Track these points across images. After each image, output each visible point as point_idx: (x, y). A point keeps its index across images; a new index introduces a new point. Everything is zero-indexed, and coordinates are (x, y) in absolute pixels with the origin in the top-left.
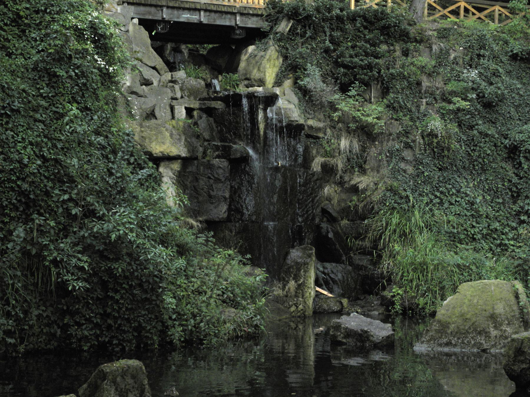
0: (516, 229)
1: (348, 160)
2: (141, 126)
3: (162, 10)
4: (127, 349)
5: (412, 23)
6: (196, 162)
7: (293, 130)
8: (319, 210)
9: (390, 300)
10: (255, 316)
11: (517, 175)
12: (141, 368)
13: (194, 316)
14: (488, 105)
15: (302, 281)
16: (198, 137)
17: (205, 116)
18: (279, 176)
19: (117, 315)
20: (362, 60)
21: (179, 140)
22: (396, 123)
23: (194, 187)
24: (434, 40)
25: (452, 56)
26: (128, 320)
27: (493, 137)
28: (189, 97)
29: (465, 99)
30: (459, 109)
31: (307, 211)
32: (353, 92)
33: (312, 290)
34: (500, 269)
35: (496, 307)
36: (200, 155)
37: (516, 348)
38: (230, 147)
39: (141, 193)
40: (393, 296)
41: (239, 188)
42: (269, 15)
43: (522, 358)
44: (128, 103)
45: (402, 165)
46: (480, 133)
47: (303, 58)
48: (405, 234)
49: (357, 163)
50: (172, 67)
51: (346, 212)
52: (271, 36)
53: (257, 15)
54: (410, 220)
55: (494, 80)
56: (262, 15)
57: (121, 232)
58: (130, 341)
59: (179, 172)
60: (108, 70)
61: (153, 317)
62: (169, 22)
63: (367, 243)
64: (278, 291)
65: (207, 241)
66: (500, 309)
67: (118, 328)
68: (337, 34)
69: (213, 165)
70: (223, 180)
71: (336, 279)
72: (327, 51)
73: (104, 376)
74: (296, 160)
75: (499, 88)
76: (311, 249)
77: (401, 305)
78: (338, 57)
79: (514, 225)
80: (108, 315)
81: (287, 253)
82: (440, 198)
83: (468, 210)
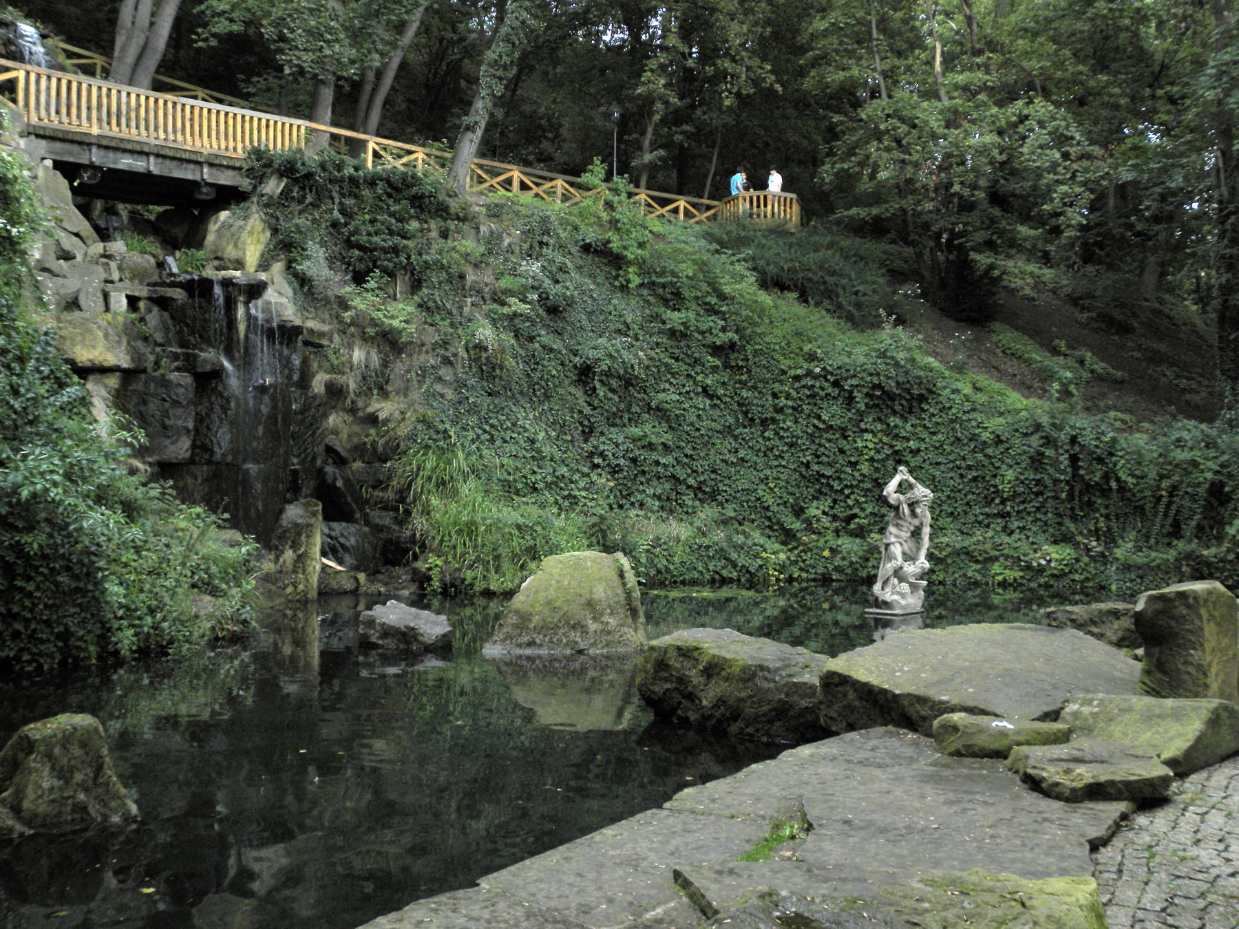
0: (588, 475)
1: (364, 378)
2: (59, 320)
3: (90, 150)
4: (46, 667)
5: (452, 195)
6: (143, 376)
7: (287, 334)
8: (321, 448)
9: (424, 575)
10: (243, 607)
11: (589, 404)
12: (96, 729)
13: (152, 611)
14: (553, 310)
15: (302, 550)
16: (146, 339)
17: (156, 309)
18: (266, 399)
19: (29, 615)
20: (384, 240)
21: (119, 342)
22: (431, 329)
23: (141, 413)
24: (482, 219)
25: (506, 243)
26: (48, 623)
27: (560, 352)
28: (131, 279)
29: (523, 301)
30: (515, 315)
31: (306, 449)
32: (372, 284)
33: (318, 562)
34: (570, 529)
35: (594, 590)
36: (150, 366)
37: (657, 660)
38: (195, 356)
39: (64, 422)
40: (430, 569)
41: (208, 415)
42: (251, 169)
43: (666, 675)
44: (37, 286)
45: (438, 387)
46: (543, 347)
47: (301, 232)
48: (444, 483)
49: (378, 384)
50: (104, 235)
51: (359, 450)
52: (255, 199)
53: (234, 168)
54: (450, 463)
55: (560, 277)
56: (240, 169)
57: (39, 487)
58: (50, 655)
59: (117, 390)
60: (9, 232)
61: (89, 616)
62: (99, 168)
63: (390, 495)
64: (268, 566)
65: (163, 494)
66: (600, 592)
67: (30, 637)
68: (349, 202)
69: (169, 381)
70: (185, 403)
71: (348, 544)
72: (335, 225)
73: (29, 746)
74: (289, 377)
75: (568, 289)
76: (316, 505)
77: (441, 580)
78: (352, 234)
79: (586, 470)
80: (15, 616)
81: (281, 511)
82: (490, 433)
83: (527, 450)
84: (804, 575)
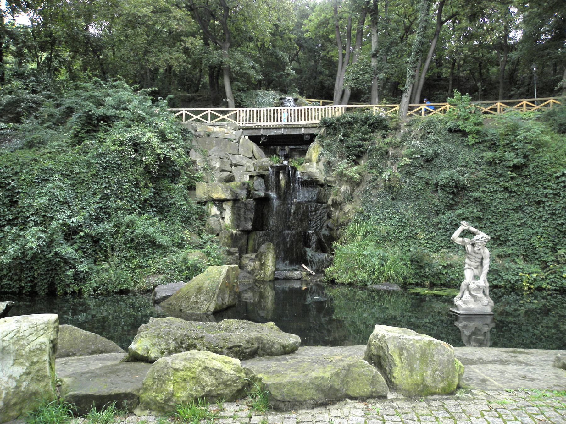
59: (232, 207)
62: (265, 136)
84: (549, 287)
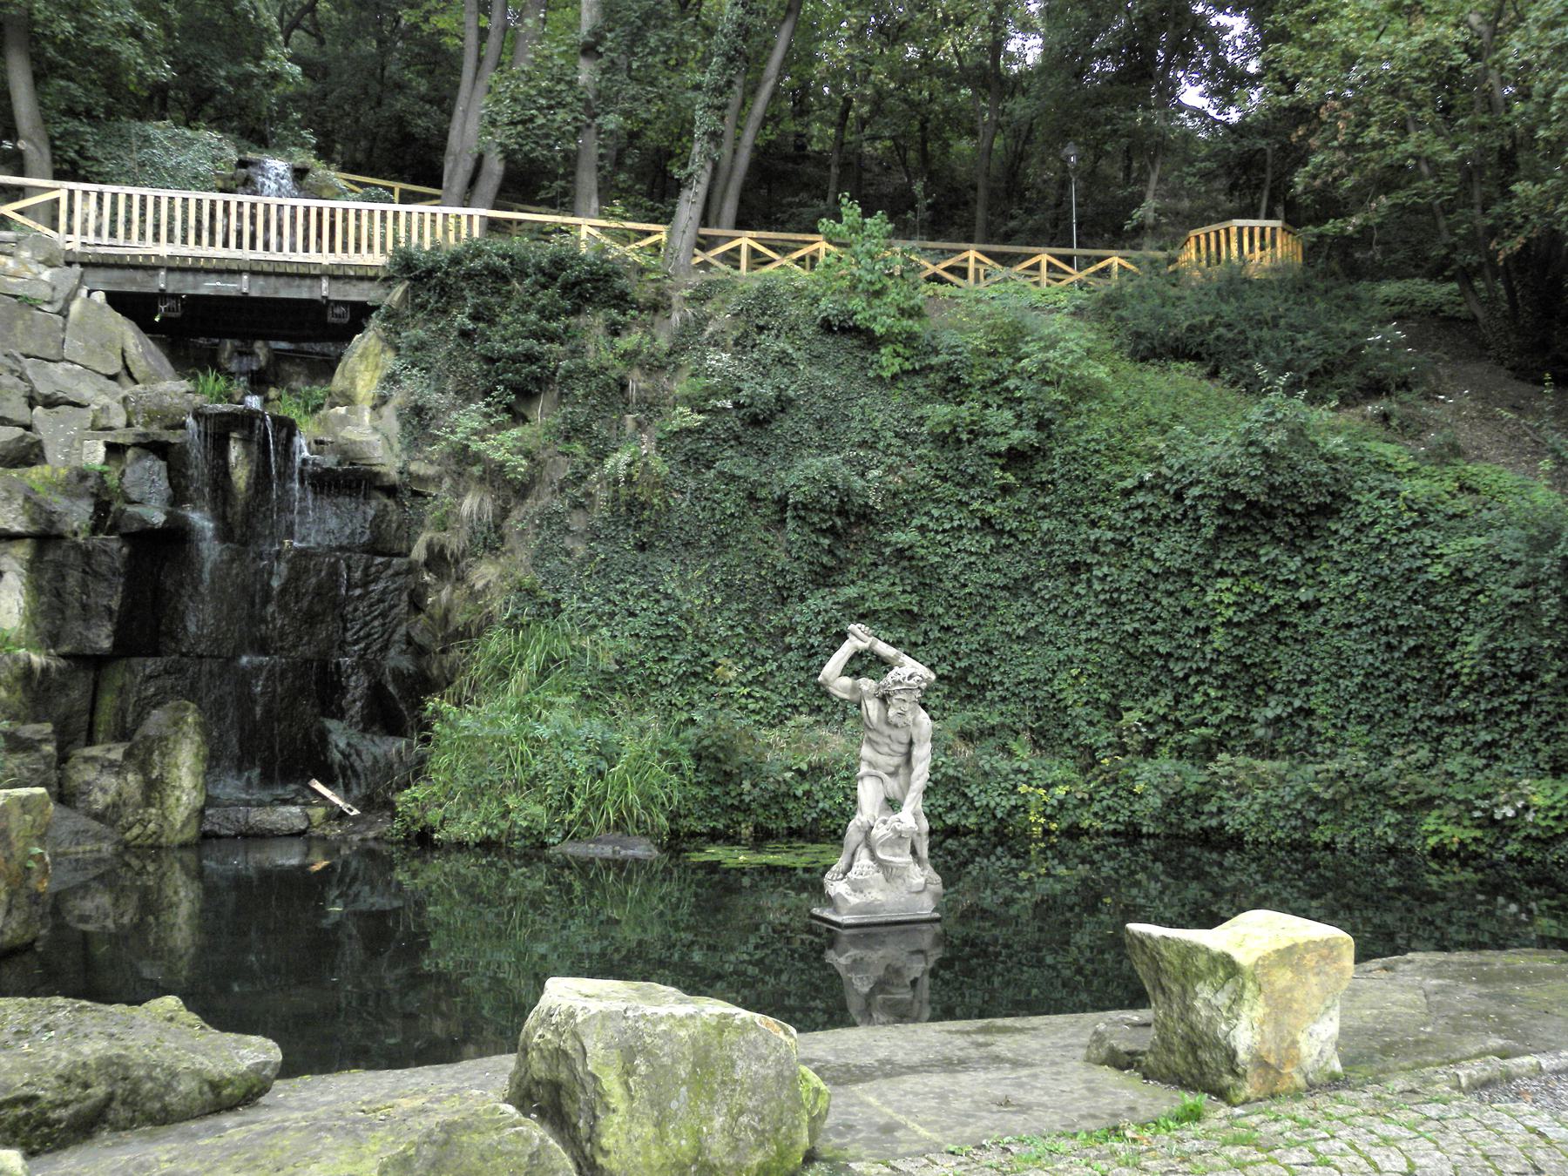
53: (372, 279)
